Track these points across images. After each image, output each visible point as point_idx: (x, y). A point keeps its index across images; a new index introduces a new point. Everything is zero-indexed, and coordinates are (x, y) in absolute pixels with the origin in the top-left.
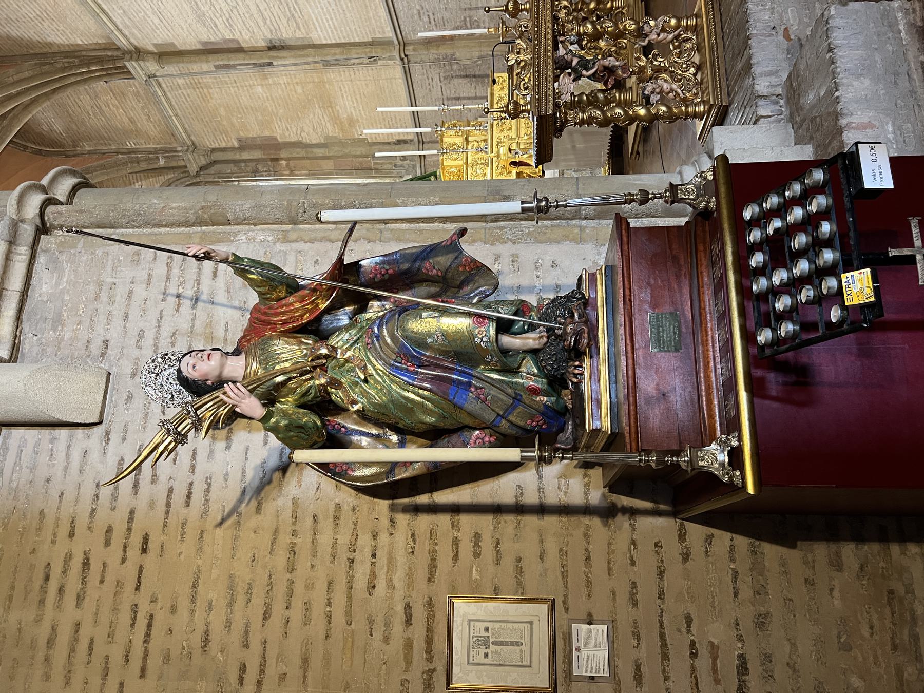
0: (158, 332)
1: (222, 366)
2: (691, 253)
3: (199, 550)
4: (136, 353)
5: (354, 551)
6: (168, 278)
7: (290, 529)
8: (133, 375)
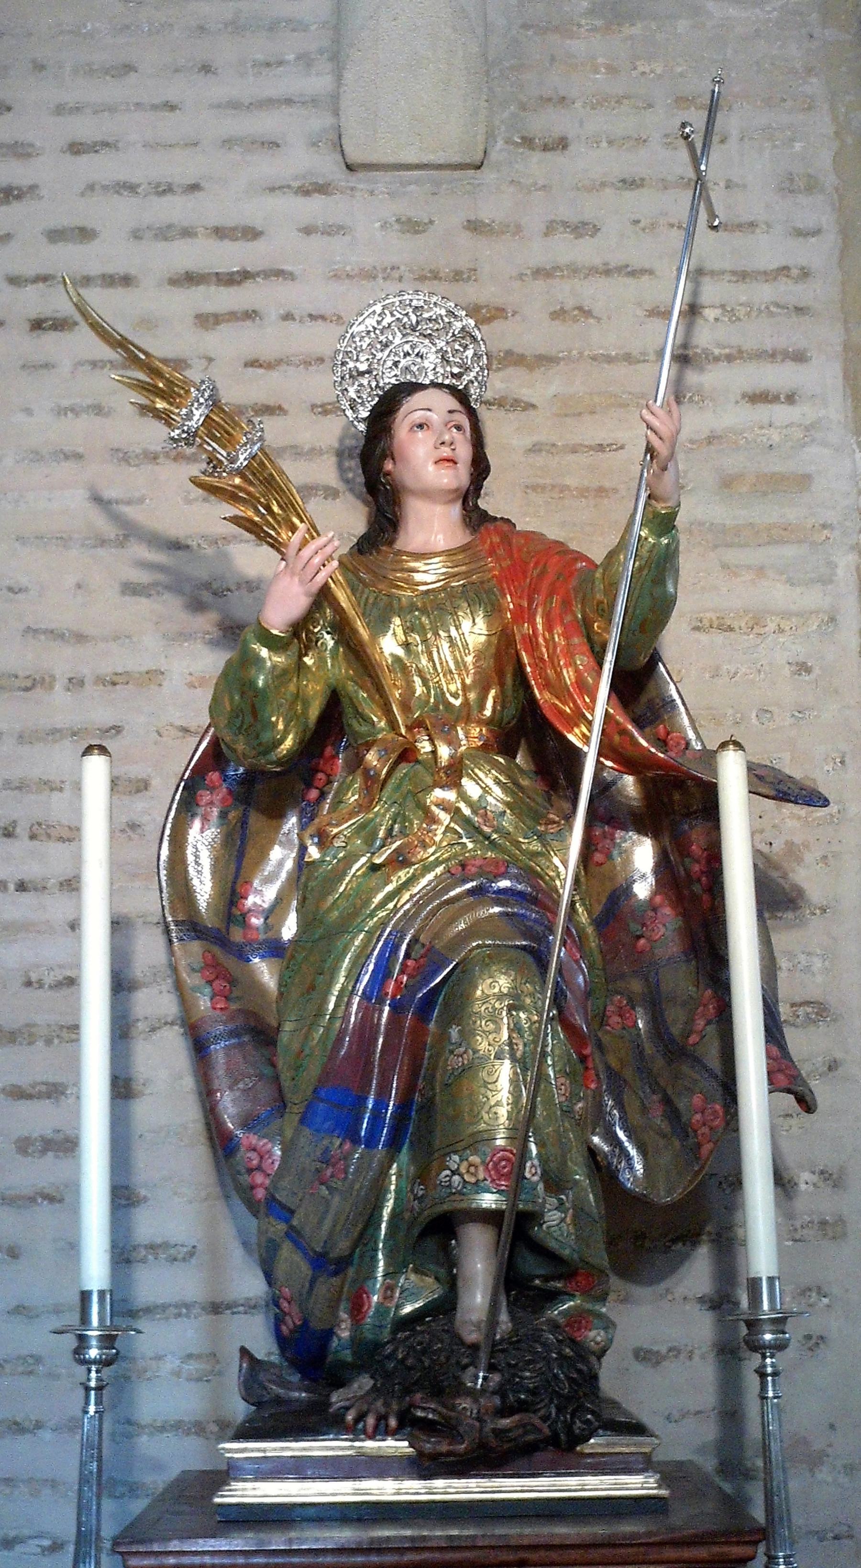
0: (593, 271)
1: (427, 494)
2: (441, 663)
3: (37, 456)
4: (534, 223)
5: (33, 837)
6: (743, 276)
7: (86, 671)
8: (475, 227)
